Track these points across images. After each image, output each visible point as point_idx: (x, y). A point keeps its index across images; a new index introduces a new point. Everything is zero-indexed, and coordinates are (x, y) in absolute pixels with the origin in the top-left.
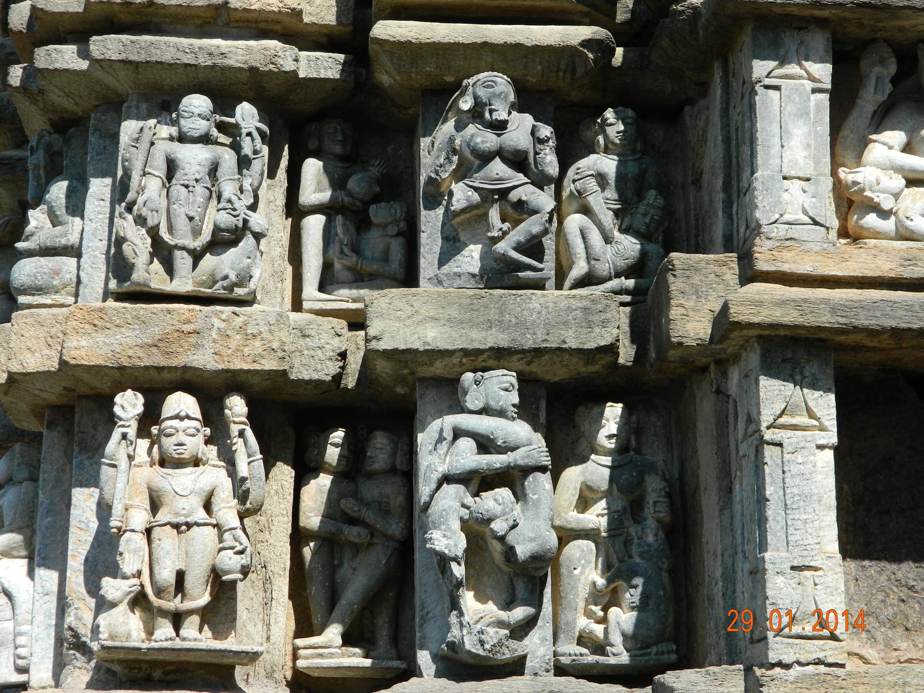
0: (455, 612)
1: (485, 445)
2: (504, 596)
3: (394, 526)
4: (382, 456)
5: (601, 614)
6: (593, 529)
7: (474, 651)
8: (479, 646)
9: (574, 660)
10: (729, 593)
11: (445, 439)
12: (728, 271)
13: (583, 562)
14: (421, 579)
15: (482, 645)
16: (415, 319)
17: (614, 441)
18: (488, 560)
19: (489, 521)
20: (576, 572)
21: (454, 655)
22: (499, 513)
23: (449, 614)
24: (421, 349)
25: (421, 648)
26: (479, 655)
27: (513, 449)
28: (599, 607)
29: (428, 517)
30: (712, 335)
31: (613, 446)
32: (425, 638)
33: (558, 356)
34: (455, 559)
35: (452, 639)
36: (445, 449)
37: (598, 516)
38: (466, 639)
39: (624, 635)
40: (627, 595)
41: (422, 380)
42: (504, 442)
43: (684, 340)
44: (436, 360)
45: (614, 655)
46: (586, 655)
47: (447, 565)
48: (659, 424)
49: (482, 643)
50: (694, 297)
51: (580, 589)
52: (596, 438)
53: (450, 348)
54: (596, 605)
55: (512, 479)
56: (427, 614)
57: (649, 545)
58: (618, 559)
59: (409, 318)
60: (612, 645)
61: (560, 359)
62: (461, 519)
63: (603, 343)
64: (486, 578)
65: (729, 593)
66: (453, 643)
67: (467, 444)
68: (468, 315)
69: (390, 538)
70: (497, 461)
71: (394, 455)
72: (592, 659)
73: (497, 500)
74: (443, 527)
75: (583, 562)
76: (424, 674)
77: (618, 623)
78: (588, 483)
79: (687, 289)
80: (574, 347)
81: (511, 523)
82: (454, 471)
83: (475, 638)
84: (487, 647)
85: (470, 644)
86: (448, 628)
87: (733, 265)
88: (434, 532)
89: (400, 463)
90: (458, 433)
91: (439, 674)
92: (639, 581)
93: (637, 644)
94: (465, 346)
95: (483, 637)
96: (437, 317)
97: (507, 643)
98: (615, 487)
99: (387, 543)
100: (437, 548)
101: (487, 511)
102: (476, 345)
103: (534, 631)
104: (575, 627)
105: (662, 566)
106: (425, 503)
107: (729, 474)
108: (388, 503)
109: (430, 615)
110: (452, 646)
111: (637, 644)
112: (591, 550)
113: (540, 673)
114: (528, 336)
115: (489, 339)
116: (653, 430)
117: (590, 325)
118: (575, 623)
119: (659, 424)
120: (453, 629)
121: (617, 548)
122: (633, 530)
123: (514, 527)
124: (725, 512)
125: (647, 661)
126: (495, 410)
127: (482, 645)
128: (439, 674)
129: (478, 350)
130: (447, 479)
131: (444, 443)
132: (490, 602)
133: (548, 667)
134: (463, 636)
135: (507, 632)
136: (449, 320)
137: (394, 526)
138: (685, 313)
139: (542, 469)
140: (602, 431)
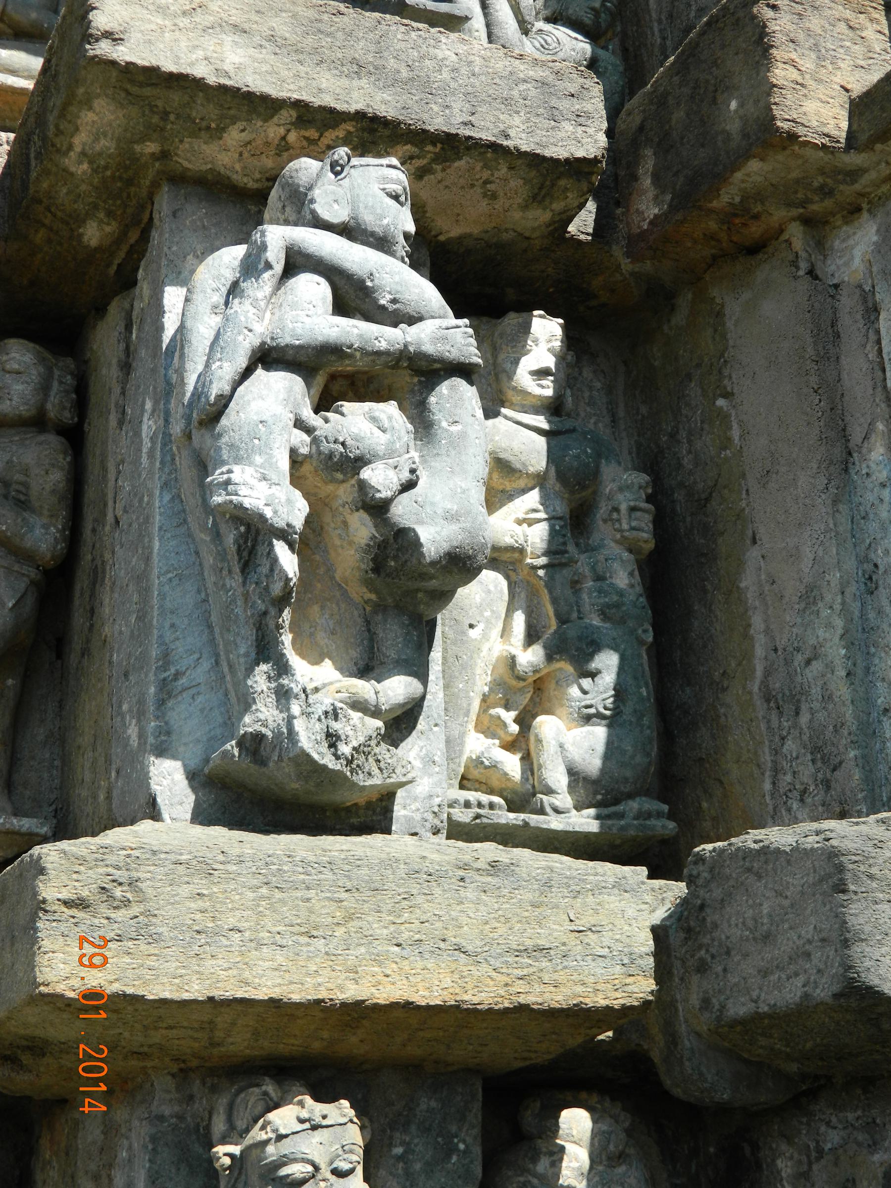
0: (264, 667)
1: (352, 296)
2: (354, 653)
3: (38, 532)
4: (20, 387)
5: (514, 728)
6: (510, 549)
7: (316, 756)
8: (324, 748)
9: (478, 816)
10: (860, 672)
11: (269, 266)
12: (868, 24)
13: (487, 614)
14: (162, 596)
15: (333, 745)
16: (198, 18)
17: (548, 382)
18: (322, 571)
19: (360, 462)
20: (473, 634)
21: (254, 768)
22: (381, 450)
23: (250, 671)
24: (212, 80)
25: (162, 752)
26: (325, 767)
27: (413, 320)
28: (513, 714)
29: (220, 435)
30: (850, 132)
31: (549, 392)
32: (168, 733)
33: (486, 166)
34: (284, 534)
35: (258, 727)
36: (268, 289)
37: (520, 522)
38: (299, 725)
39: (573, 773)
40: (574, 691)
41: (180, 180)
42: (394, 301)
43: (800, 130)
44: (234, 120)
45: (557, 811)
46: (500, 808)
47: (262, 549)
48: (598, 385)
49: (332, 739)
50: (813, 56)
51: (478, 671)
52: (511, 375)
53: (274, 92)
54: (507, 708)
55: (411, 379)
56: (177, 675)
57: (621, 593)
58: (558, 615)
59: (184, 13)
60: (549, 791)
61: (486, 174)
62: (293, 452)
63: (580, 154)
64: (316, 608)
65: (860, 672)
66: (258, 738)
67: (312, 289)
68: (310, 40)
69: (24, 556)
70: (385, 337)
71: (44, 388)
72: (513, 818)
73: (364, 423)
74: (258, 459)
75: (487, 614)
76: (166, 816)
77: (561, 746)
78: (502, 456)
79: (801, 36)
80: (524, 148)
81: (406, 475)
82: (287, 339)
83: (318, 726)
84: (345, 749)
85: (308, 738)
86: (246, 702)
87: (875, 15)
88: (236, 468)
89: (57, 406)
90: (297, 262)
91: (203, 816)
92: (608, 663)
93: (596, 793)
94: (305, 97)
95: (336, 726)
96: (246, 26)
97: (377, 750)
98: (553, 470)
99: (16, 568)
100: (247, 503)
101: (356, 439)
102: (327, 100)
103: (410, 740)
104: (461, 752)
105: (644, 636)
106: (220, 397)
107: (844, 434)
108: (26, 485)
109: (183, 681)
110: (254, 745)
111: (596, 793)
112: (501, 591)
113: (422, 832)
114: (436, 108)
115: (355, 95)
116: (587, 394)
117: (554, 116)
118: (462, 744)
119: (598, 385)
120: (260, 705)
121: (558, 591)
122: (583, 563)
123: (409, 486)
124: (841, 507)
125: (622, 828)
126: (373, 234)
127: (333, 745)
128: (203, 816)
129: (332, 111)
130: (267, 357)
131: (266, 275)
132: (328, 663)
133: (437, 822)
134: (290, 719)
135: (379, 724)
136: (271, 39)
137: (38, 532)
138: (800, 81)
139: (464, 371)
140: (524, 361)
